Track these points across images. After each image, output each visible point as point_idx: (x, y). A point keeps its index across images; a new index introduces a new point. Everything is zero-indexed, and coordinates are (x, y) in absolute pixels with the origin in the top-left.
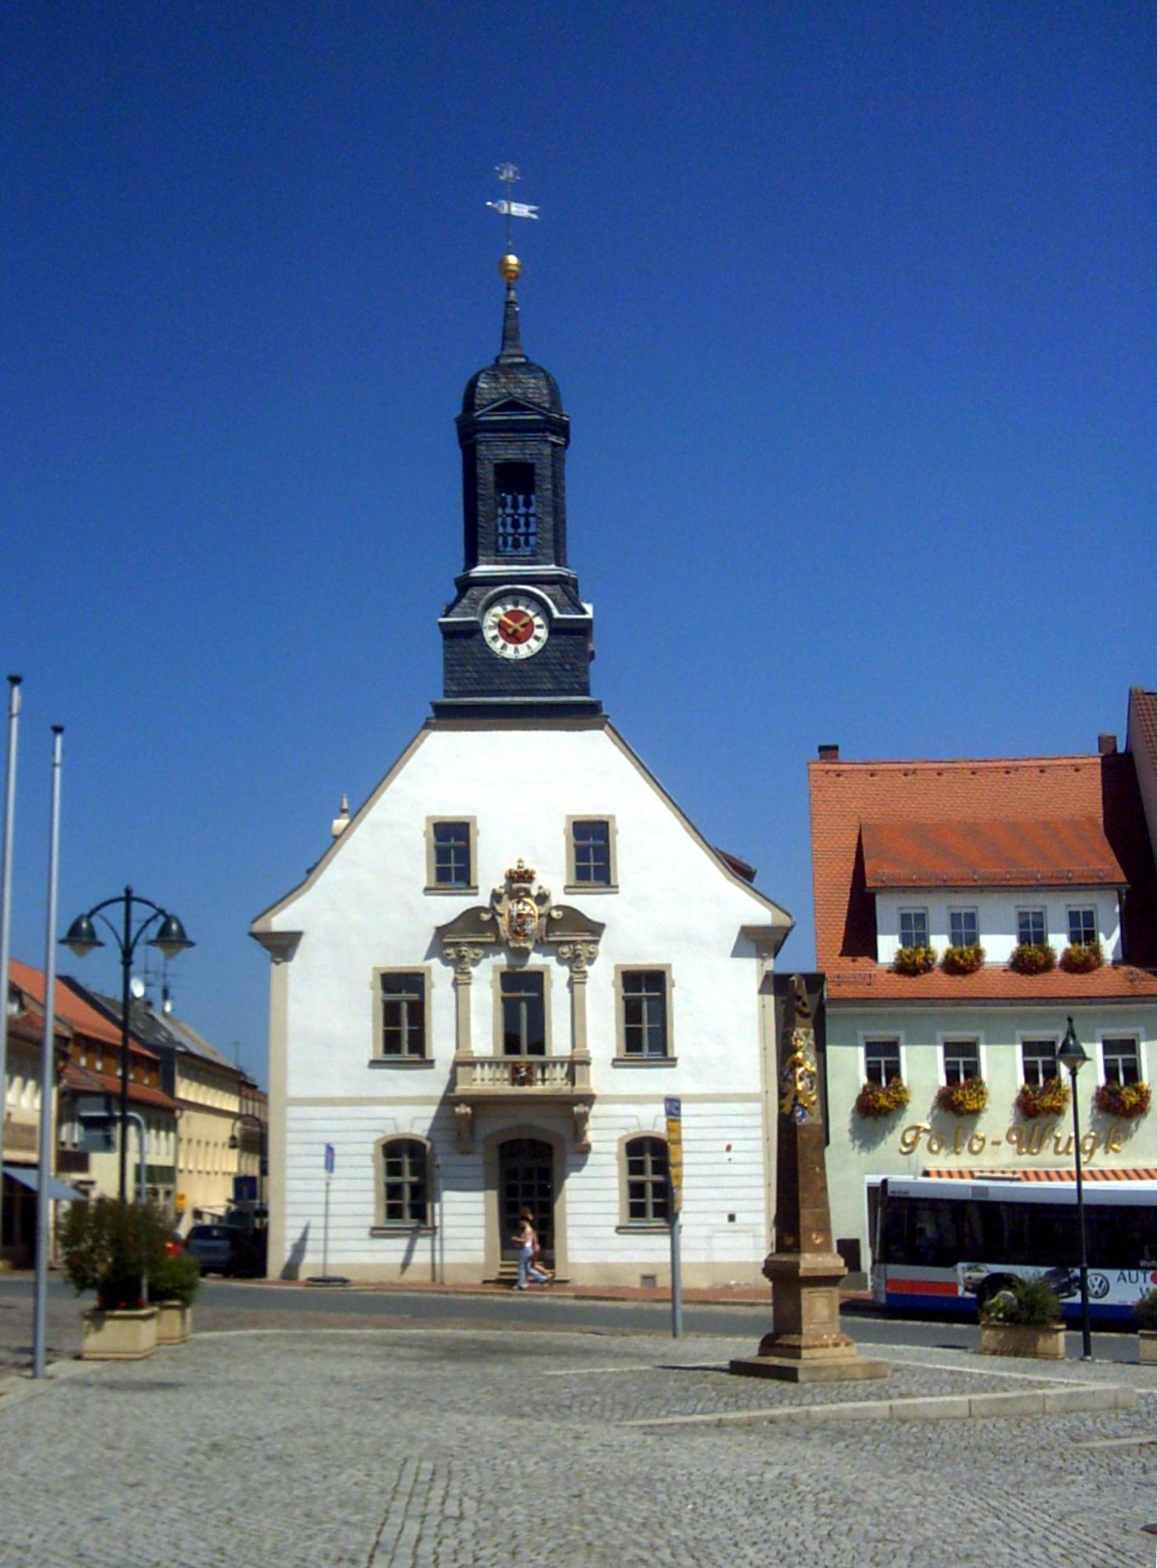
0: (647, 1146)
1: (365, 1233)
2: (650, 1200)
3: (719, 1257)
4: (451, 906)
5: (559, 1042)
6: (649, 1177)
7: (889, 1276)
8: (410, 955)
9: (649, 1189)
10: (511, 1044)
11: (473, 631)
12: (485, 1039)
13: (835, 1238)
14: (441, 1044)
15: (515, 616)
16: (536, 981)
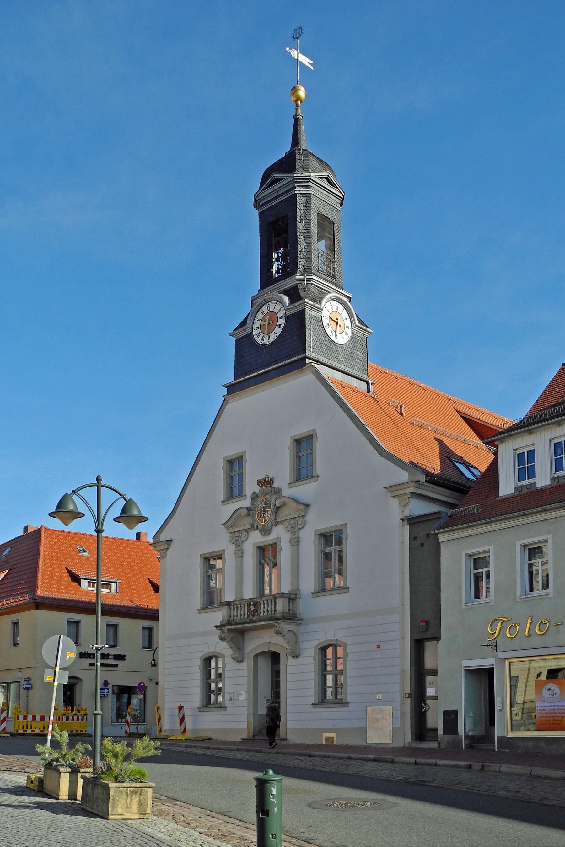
7: (442, 733)
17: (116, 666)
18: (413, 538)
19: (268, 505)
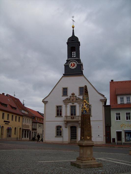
1: (54, 137)
2: (59, 133)
3: (97, 140)
4: (65, 98)
8: (62, 104)
10: (72, 115)
11: (68, 66)
12: (69, 114)
14: (63, 114)
16: (75, 106)
17: (8, 124)
18: (105, 109)
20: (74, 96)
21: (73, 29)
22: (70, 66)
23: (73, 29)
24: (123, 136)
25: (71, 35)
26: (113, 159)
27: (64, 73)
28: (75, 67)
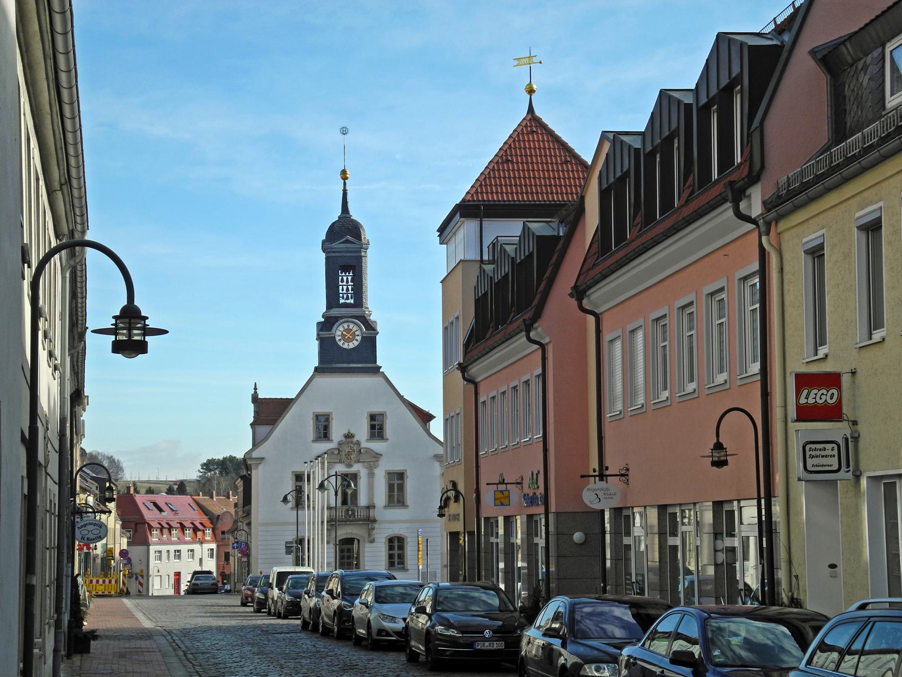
0: (325, 334)
2: (396, 560)
5: (363, 501)
6: (396, 552)
9: (396, 548)
13: (147, 338)
15: (348, 330)
16: (355, 477)
19: (349, 448)
20: (352, 442)
21: (345, 184)
22: (338, 338)
23: (345, 184)
24: (778, 508)
25: (335, 214)
26: (763, 507)
27: (317, 365)
28: (356, 343)
